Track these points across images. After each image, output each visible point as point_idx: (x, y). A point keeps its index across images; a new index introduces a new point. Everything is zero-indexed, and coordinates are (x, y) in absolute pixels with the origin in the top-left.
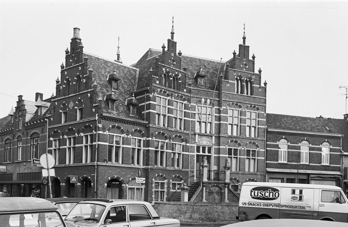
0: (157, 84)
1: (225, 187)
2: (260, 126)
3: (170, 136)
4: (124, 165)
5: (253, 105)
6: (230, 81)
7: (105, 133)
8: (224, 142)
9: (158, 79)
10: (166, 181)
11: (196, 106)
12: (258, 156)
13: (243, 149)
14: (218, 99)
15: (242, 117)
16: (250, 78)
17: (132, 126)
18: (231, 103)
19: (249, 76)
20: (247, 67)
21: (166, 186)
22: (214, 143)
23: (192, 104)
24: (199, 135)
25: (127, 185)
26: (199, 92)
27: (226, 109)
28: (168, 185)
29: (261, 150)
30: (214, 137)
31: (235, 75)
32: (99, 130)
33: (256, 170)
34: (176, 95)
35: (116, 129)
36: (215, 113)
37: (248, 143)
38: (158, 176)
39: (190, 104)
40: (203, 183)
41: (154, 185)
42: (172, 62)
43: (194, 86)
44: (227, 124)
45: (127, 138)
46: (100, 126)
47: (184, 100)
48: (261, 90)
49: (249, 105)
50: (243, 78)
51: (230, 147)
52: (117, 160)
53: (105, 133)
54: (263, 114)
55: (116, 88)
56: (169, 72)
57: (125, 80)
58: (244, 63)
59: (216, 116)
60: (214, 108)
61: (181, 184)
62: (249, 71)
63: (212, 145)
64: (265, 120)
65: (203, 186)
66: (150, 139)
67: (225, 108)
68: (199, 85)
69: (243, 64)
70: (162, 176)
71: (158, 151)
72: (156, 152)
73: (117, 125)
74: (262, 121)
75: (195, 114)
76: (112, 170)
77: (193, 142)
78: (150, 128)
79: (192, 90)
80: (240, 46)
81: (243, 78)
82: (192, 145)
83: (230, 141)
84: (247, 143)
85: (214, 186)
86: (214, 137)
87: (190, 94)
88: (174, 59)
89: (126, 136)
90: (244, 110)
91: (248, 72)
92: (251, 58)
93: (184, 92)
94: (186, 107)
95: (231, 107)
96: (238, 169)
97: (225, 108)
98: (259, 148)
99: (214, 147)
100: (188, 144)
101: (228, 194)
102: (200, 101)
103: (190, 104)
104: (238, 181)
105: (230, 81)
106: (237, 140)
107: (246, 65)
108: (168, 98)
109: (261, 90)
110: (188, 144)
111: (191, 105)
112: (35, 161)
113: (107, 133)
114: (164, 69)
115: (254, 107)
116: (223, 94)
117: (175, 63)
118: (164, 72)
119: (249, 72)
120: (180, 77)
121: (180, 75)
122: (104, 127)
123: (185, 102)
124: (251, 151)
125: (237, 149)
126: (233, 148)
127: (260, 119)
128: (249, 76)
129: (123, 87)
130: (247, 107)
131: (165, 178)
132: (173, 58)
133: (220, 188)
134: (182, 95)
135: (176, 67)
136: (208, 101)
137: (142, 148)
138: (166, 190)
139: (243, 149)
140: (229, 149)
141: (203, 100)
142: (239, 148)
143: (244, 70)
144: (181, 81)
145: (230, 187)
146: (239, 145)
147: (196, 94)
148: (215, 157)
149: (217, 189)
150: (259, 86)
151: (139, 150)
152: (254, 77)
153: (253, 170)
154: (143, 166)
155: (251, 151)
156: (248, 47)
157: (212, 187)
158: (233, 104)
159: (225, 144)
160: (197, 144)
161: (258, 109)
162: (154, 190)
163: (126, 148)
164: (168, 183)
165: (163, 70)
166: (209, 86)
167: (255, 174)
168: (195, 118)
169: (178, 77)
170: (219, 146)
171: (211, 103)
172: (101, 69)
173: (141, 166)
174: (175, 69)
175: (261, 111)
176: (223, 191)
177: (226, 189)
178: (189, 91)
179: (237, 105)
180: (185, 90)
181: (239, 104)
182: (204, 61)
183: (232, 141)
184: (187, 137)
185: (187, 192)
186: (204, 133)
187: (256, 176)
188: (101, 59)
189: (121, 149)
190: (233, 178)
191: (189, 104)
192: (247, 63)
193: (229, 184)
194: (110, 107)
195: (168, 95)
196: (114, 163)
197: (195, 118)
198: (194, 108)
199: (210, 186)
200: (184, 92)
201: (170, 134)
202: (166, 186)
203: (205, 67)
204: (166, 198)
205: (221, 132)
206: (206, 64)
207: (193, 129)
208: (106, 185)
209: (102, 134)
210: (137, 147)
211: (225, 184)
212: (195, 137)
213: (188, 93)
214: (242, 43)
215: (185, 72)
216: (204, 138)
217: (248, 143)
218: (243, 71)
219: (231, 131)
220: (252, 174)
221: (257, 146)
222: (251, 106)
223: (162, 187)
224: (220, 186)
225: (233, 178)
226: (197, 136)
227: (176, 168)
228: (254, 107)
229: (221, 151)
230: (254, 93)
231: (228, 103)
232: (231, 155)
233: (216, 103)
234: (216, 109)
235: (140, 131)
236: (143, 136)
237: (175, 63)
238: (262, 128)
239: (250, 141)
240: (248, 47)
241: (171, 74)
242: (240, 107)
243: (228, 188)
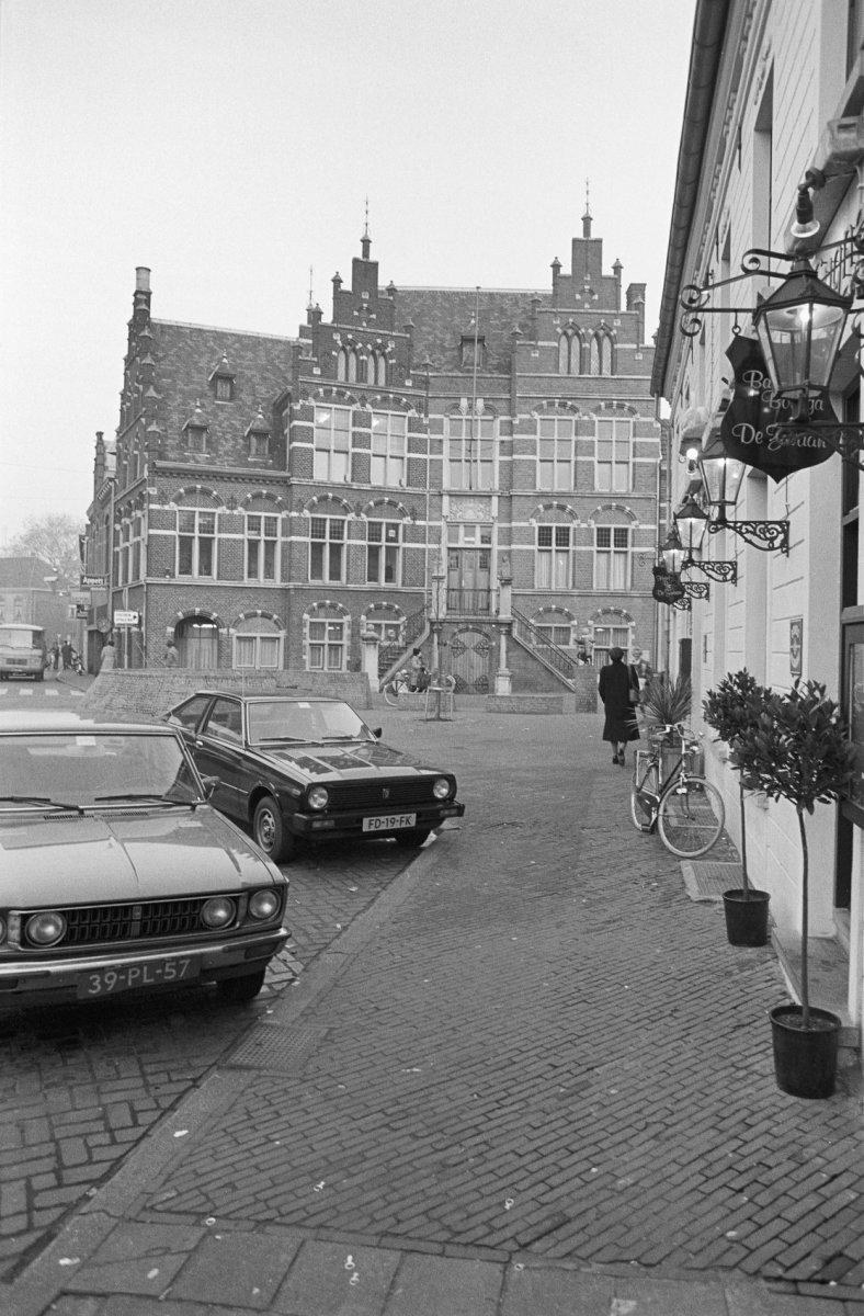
0: (315, 376)
1: (500, 632)
2: (638, 460)
3: (358, 505)
4: (220, 583)
5: (615, 402)
6: (540, 343)
7: (166, 507)
8: (526, 510)
9: (317, 364)
10: (347, 619)
11: (446, 420)
12: (633, 546)
13: (584, 526)
14: (508, 396)
15: (580, 438)
16: (607, 329)
17: (243, 486)
18: (544, 402)
19: (603, 321)
20: (596, 297)
21: (347, 631)
22: (495, 513)
23: (431, 416)
24: (450, 496)
25: (232, 631)
26: (451, 382)
27: (530, 421)
28: (353, 630)
29: (641, 527)
30: (495, 500)
31: (557, 326)
32: (150, 502)
33: (629, 584)
34: (379, 397)
35: (199, 498)
36: (501, 434)
37: (599, 508)
38: (321, 606)
39: (426, 416)
40: (432, 624)
41: (306, 630)
42: (364, 315)
43: (450, 367)
44: (591, 463)
45: (232, 516)
46: (153, 491)
47: (407, 408)
48: (641, 358)
49: (603, 404)
50: (583, 330)
51: (544, 521)
52: (269, 574)
53: (166, 507)
54: (652, 424)
55: (228, 395)
56: (352, 343)
57: (267, 375)
58: (587, 287)
59: (502, 442)
60: (498, 422)
61: (398, 626)
62: (602, 308)
63: (491, 521)
64: (658, 440)
65: (432, 631)
66: (294, 514)
67: (527, 416)
68: (466, 364)
69: (582, 292)
70: (333, 606)
71: (324, 544)
72: (318, 548)
73: (199, 486)
74: (646, 443)
75: (441, 441)
76: (186, 595)
77: (436, 515)
78: (294, 487)
79: (432, 380)
80: (356, 261)
81: (583, 330)
82: (431, 523)
83: (541, 506)
84: (597, 511)
85: (467, 629)
86: (495, 500)
87: (426, 389)
88: (371, 307)
89: (228, 512)
90: (586, 418)
91: (599, 311)
92: (607, 271)
93: (404, 386)
94: (414, 425)
95: (548, 414)
96: (571, 584)
97: (527, 416)
98: (637, 522)
99: (497, 525)
100: (418, 523)
101: (507, 652)
102: (456, 406)
103: (426, 416)
104: (570, 617)
105: (540, 343)
106: (563, 502)
107: (592, 292)
108: (354, 408)
109: (641, 358)
110: (418, 523)
111: (430, 420)
112: (85, 580)
113: (172, 506)
114: (337, 337)
115: (621, 407)
116: (520, 382)
117: (374, 316)
118: (339, 342)
119: (603, 311)
120: (389, 349)
121: (391, 346)
122: (163, 493)
123: (412, 413)
124: (263, 519)
125: (626, 530)
126: (554, 525)
127: (638, 439)
128: (603, 321)
129: (254, 391)
130: (597, 410)
131: (343, 612)
132: (365, 305)
133: (486, 635)
134: (400, 397)
135: (377, 326)
136: (480, 404)
137: (280, 539)
138: (346, 642)
139: (584, 526)
140: (540, 528)
141: (464, 403)
142: (631, 527)
143: (587, 306)
144: (394, 361)
145: (515, 634)
146: (573, 515)
147: (444, 389)
148: (500, 552)
149: (478, 638)
150: (635, 346)
151: (270, 545)
152: (617, 323)
153: (622, 584)
154: (330, 579)
155: (263, 519)
156: (376, 264)
157: (461, 631)
158: (551, 404)
159: (523, 516)
160: (448, 520)
161: (632, 411)
162: (307, 641)
163: (228, 540)
164: (355, 625)
165: (335, 338)
166: (495, 362)
167: (624, 596)
168: (441, 453)
169: (387, 351)
170: (510, 522)
171: (487, 407)
172: (201, 355)
173: (277, 583)
174: (373, 330)
175: (643, 415)
176: (494, 644)
177: (503, 638)
178: (425, 383)
179: (563, 405)
180: (409, 383)
181: (570, 403)
182: (503, 296)
183: (548, 507)
184: (415, 502)
185: (372, 646)
186: (468, 489)
187: (627, 600)
188: (208, 331)
189: (345, 548)
190: (554, 607)
191: (422, 416)
192: (595, 288)
193: (510, 625)
194: (190, 445)
195: (352, 401)
196: (196, 577)
197: (441, 453)
198: (437, 426)
199: (456, 630)
200: (404, 386)
201: (356, 498)
202: (347, 631)
203: (502, 311)
204: (348, 662)
205: (517, 485)
206: (507, 304)
207: (437, 481)
208: (171, 630)
209: (159, 511)
210: (263, 537)
211: (499, 624)
212: (441, 501)
213: (421, 388)
214: (580, 235)
215: (408, 336)
216: (470, 504)
217: (599, 508)
218: (582, 311)
219: (554, 478)
220: (614, 595)
221: (631, 517)
222: (609, 406)
223: (338, 633)
224: (486, 629)
225: (554, 607)
226: (446, 499)
227: (383, 583)
228: (621, 407)
229: (516, 536)
230: (620, 368)
231: (537, 403)
232: (609, 546)
233: (503, 405)
234: (501, 422)
235: (270, 497)
236: (280, 507)
237: (374, 316)
238: (646, 465)
239: (606, 502)
240: (376, 264)
241: (360, 345)
242: (574, 410)
243: (509, 633)
